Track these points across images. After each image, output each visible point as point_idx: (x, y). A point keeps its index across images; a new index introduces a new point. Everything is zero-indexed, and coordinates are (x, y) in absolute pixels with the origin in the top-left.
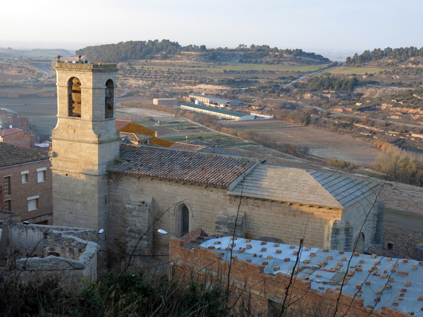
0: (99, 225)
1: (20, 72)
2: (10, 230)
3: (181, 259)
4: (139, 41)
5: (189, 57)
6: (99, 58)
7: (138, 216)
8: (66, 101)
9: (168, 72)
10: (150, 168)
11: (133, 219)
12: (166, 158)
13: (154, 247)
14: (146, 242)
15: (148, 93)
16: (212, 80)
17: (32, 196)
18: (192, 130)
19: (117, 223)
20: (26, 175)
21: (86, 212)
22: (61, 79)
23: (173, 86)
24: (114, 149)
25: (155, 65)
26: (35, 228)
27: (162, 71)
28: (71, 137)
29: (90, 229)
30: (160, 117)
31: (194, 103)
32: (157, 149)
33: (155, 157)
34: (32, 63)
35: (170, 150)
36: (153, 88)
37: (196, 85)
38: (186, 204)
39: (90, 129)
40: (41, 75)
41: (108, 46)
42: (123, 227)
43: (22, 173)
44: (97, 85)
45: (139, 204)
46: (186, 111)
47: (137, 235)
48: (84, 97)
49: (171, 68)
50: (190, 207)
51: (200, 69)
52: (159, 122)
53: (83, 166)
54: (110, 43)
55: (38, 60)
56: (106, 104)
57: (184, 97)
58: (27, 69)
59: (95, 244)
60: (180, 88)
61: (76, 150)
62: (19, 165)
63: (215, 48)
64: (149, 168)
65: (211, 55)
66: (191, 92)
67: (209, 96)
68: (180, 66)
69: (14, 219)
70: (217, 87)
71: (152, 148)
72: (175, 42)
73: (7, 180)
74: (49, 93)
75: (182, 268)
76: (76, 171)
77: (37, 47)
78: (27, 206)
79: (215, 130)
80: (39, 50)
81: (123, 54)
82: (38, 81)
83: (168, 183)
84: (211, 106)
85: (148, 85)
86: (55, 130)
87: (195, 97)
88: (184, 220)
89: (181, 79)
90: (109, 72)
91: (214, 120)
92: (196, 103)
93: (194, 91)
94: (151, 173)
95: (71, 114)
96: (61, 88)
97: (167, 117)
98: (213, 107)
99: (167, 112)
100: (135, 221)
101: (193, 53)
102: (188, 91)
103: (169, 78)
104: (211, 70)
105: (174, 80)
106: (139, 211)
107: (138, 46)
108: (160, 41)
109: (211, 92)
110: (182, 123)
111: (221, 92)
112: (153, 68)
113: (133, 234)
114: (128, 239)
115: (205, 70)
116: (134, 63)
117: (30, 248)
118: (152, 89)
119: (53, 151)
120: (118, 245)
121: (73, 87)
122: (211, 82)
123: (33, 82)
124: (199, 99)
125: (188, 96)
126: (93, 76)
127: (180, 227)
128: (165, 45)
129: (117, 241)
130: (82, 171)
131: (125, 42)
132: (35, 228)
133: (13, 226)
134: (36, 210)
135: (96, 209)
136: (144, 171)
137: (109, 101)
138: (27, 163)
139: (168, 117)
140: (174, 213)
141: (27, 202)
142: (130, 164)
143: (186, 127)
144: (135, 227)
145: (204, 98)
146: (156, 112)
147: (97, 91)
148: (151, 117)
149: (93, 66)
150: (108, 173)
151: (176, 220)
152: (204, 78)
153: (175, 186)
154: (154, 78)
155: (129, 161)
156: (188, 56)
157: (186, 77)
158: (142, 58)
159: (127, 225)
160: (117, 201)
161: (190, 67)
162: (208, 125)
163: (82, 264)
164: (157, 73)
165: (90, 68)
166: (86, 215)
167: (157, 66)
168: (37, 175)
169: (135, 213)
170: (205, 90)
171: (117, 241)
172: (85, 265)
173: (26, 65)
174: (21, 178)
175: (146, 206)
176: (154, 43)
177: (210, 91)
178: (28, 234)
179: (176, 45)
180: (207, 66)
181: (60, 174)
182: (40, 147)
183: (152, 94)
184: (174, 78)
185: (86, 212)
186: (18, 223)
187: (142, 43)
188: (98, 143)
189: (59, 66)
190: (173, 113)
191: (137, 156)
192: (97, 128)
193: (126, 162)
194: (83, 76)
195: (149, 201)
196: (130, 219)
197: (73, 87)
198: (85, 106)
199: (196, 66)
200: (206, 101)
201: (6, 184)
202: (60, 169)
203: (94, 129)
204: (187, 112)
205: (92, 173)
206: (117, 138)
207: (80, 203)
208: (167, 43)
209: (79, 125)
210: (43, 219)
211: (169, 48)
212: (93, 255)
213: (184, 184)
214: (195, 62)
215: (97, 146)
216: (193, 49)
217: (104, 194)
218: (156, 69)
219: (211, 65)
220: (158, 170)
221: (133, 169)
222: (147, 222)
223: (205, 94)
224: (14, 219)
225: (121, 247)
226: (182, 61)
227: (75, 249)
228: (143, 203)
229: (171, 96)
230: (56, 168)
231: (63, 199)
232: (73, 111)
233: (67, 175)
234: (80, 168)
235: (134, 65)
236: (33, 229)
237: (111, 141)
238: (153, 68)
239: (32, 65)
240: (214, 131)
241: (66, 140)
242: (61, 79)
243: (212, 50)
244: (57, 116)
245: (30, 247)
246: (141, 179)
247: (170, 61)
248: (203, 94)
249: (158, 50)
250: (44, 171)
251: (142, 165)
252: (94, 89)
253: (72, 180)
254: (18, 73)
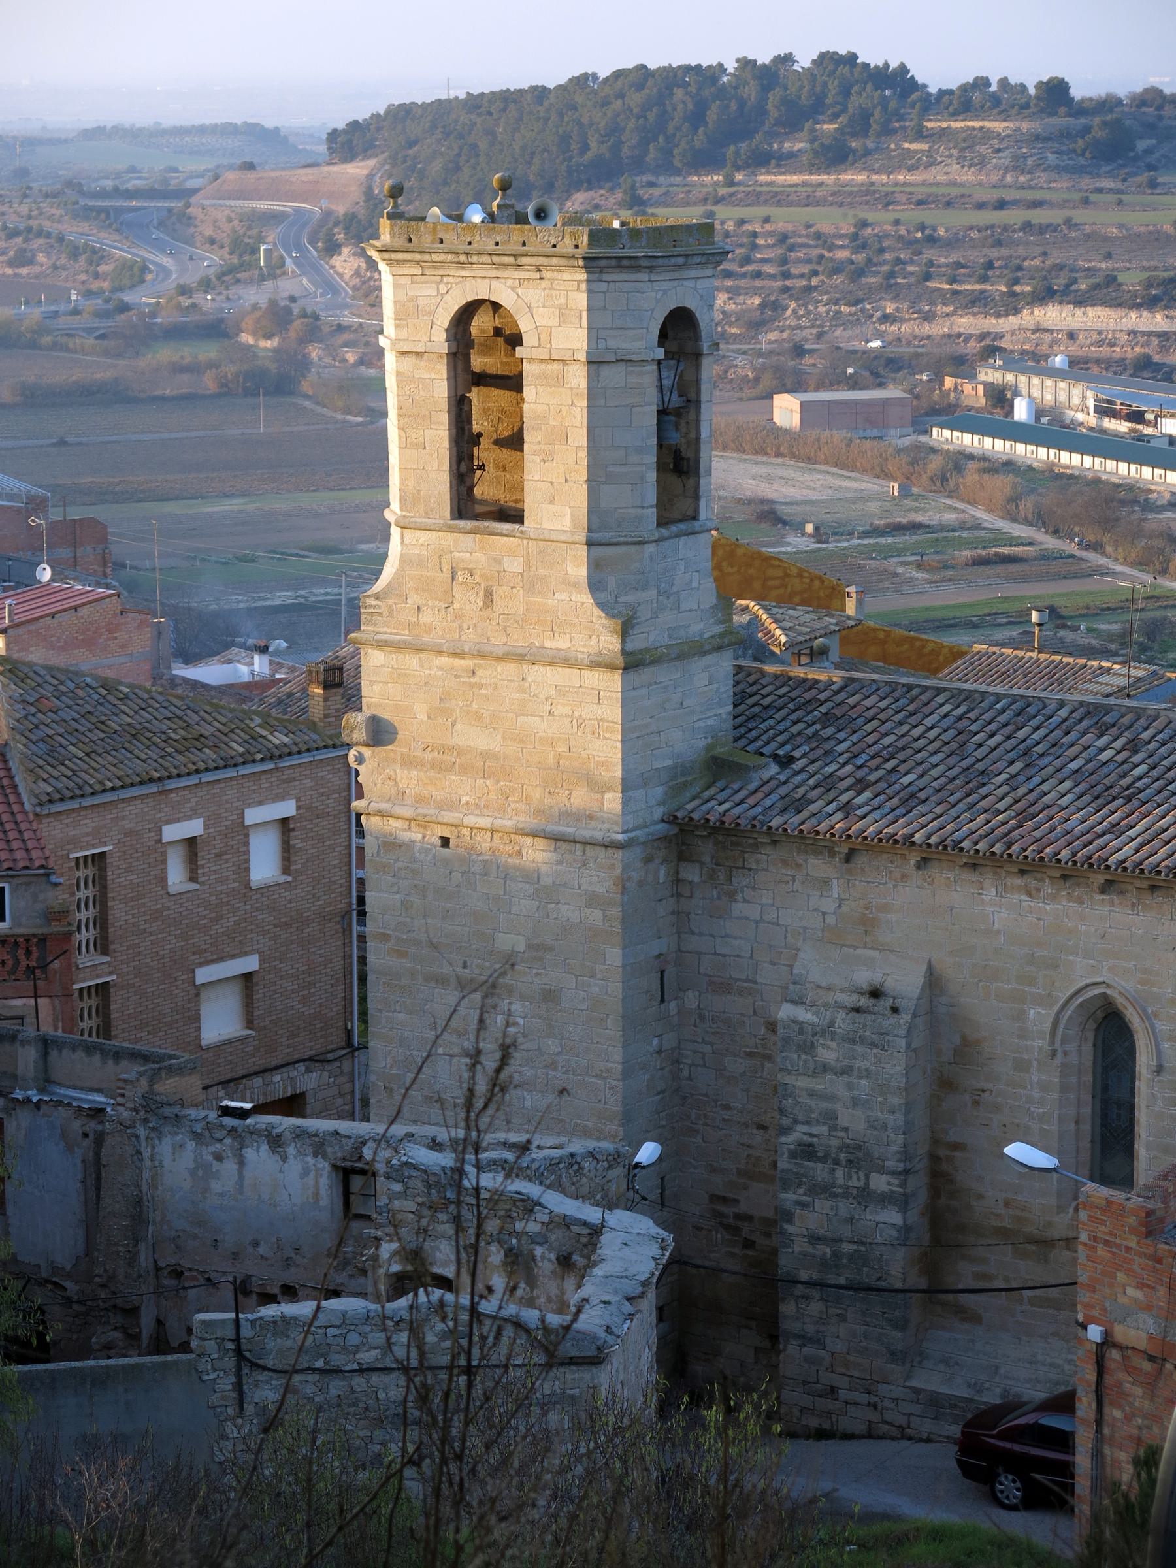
0: (627, 1118)
1: (23, 259)
2: (146, 1151)
3: (1148, 1308)
4: (687, 69)
5: (970, 148)
6: (458, 168)
7: (846, 1071)
8: (439, 434)
9: (857, 242)
10: (911, 800)
11: (818, 1085)
12: (992, 742)
13: (936, 1241)
14: (893, 1216)
15: (740, 360)
16: (1111, 280)
17: (221, 959)
18: (1000, 568)
19: (727, 1107)
20: (191, 842)
21: (552, 1045)
22: (408, 313)
23: (885, 318)
24: (703, 697)
25: (779, 204)
26: (288, 1136)
27: (818, 236)
28: (470, 636)
29: (592, 1144)
30: (815, 496)
31: (1010, 411)
32: (939, 691)
33: (932, 734)
34: (87, 209)
35: (1014, 699)
36: (772, 336)
37: (1017, 311)
38: (1120, 1001)
39: (575, 585)
40: (137, 274)
41: (507, 99)
42: (762, 1127)
43: (173, 832)
44: (612, 344)
45: (850, 999)
46: (960, 459)
47: (840, 1173)
48: (541, 408)
49: (871, 217)
50: (1145, 1016)
51: (1039, 217)
52: (809, 528)
53: (537, 794)
54: (519, 78)
55: (117, 192)
56: (660, 446)
57: (949, 382)
58: (61, 239)
59: (643, 1224)
60: (926, 329)
61: (497, 705)
62: (154, 788)
63: (1122, 92)
64: (903, 802)
65: (1098, 133)
66: (991, 350)
67: (1095, 370)
68: (920, 203)
69: (168, 1086)
70: (1136, 320)
71: (910, 688)
72: (893, 65)
73: (90, 872)
74: (185, 377)
75: (1152, 1358)
76: (498, 822)
77: (108, 117)
78: (197, 1019)
79: (1132, 565)
80: (119, 132)
81: (593, 144)
82: (124, 308)
83: (1018, 881)
84: (1104, 431)
85: (739, 316)
86: (377, 597)
87: (1010, 377)
88: (1105, 1089)
89: (928, 277)
90: (678, 267)
91: (1124, 512)
92: (1021, 411)
93: (1004, 344)
94: (919, 826)
95: (466, 505)
96: (409, 361)
97: (855, 500)
98: (1117, 435)
99: (853, 468)
100: (832, 1098)
101: (998, 126)
102: (973, 347)
103: (860, 272)
104: (1104, 219)
105: (889, 286)
106: (852, 1041)
107: (679, 93)
108: (804, 60)
109: (1105, 351)
110: (942, 528)
111: (1163, 349)
112: (767, 220)
113: (820, 1171)
114: (789, 1197)
115: (1068, 221)
116: (656, 192)
117: (261, 1250)
118: (769, 338)
119: (366, 712)
120: (736, 1231)
121: (482, 356)
122: (1105, 291)
123: (100, 314)
124: (1036, 393)
125: (972, 376)
126: (590, 292)
127: (1087, 1127)
128: (833, 87)
129: (728, 1210)
130: (532, 822)
131: (604, 73)
132: (288, 1136)
133: (167, 1129)
134: (242, 1040)
135: (612, 1029)
136: (876, 815)
137: (677, 427)
138: (193, 780)
139: (870, 499)
140: (1054, 1054)
141: (197, 991)
142: (798, 779)
143: (967, 553)
144: (833, 1128)
145: (1062, 385)
146: (791, 474)
147: (614, 375)
148: (763, 501)
149: (593, 236)
150: (675, 830)
151: (1064, 1088)
152: (1060, 267)
153: (1054, 898)
154: (773, 277)
155: (786, 762)
156: (969, 141)
157: (959, 265)
158: (704, 160)
159: (785, 1121)
160: (723, 987)
161: (981, 206)
162: (1091, 538)
163: (595, 1337)
164: (791, 248)
165: (571, 250)
166: (553, 1066)
167: (790, 204)
168: (247, 844)
169: (829, 1053)
170: (1072, 335)
171: (728, 1210)
172: (610, 1339)
173: (50, 218)
174: (164, 862)
175: (895, 1010)
176: (771, 75)
177: (1100, 343)
178: (248, 1173)
179: (898, 81)
180: (1076, 196)
181: (407, 836)
182: (205, 686)
183: (764, 368)
184: (891, 275)
185: (552, 1045)
186: (193, 1113)
187: (704, 77)
188: (620, 662)
189: (401, 242)
190: (890, 477)
191: (830, 731)
192: (612, 582)
193: (774, 769)
194: (533, 294)
195: (906, 982)
196: (803, 1083)
197: (482, 356)
198: (548, 457)
199: (1015, 203)
200: (1079, 403)
201: (82, 894)
202: (408, 812)
203: (595, 586)
204: (971, 465)
205: (585, 834)
206: (722, 635)
207: (522, 997)
208: (844, 70)
209: (514, 565)
210: (280, 1085)
211: (855, 102)
212: (645, 1284)
213: (1107, 887)
214: (1009, 179)
215: (613, 682)
216: (996, 100)
217: (656, 947)
218: (781, 226)
219: (1100, 191)
220: (953, 812)
221: (813, 808)
222: (896, 1100)
223: (1073, 362)
224: (168, 1086)
225: (749, 1244)
226: (935, 174)
227: (539, 1251)
228: (876, 993)
229: (877, 375)
230: (384, 806)
231: (428, 979)
232: (477, 491)
233: (445, 842)
234: (521, 806)
235: (658, 204)
236: (275, 1142)
237: (688, 651)
238: (767, 220)
239: (86, 218)
240: (1125, 577)
241: (440, 652)
242: (408, 313)
243: (1108, 104)
244: (387, 514)
245: (256, 1244)
246: (861, 860)
247: (861, 178)
248: (1059, 361)
249: (797, 116)
250: (284, 821)
251: (861, 785)
252: (594, 363)
253: (476, 869)
254: (11, 263)
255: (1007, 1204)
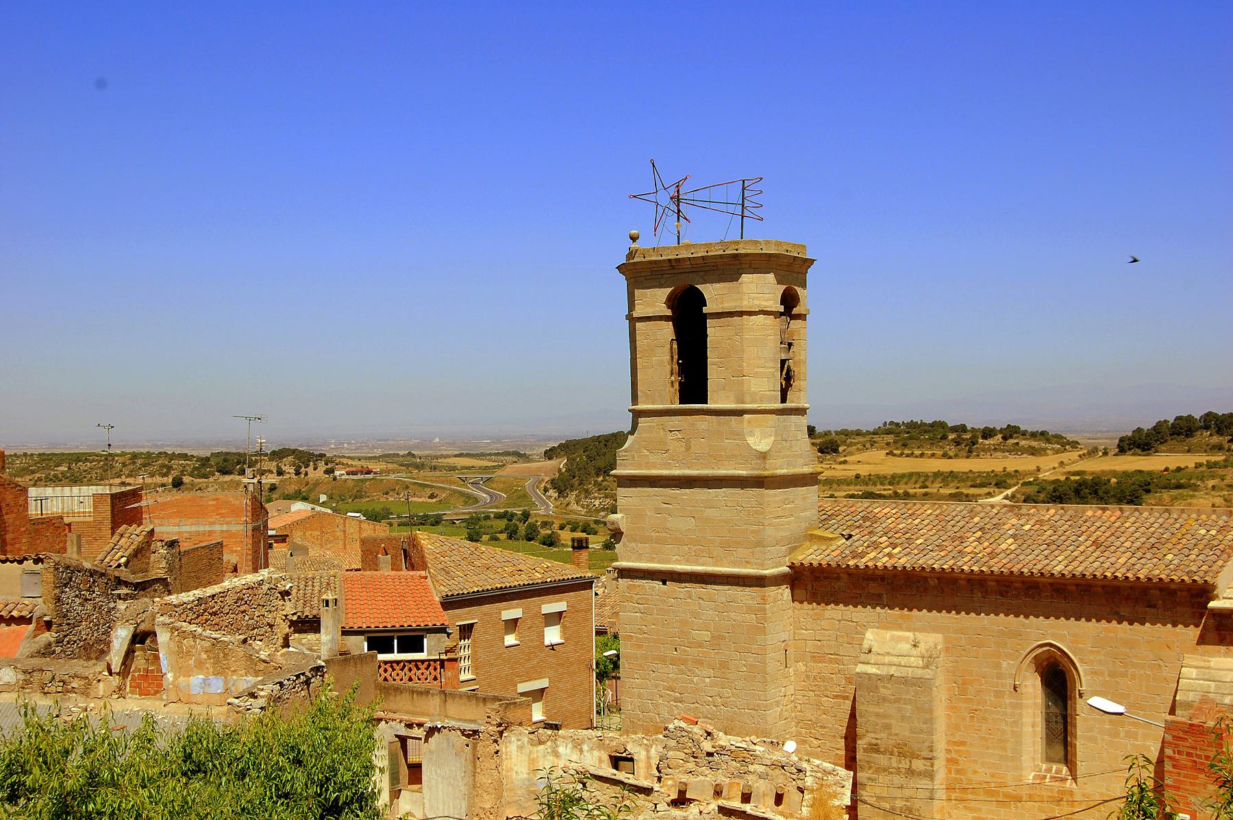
7: (898, 701)
196: (872, 709)
255: (992, 776)
